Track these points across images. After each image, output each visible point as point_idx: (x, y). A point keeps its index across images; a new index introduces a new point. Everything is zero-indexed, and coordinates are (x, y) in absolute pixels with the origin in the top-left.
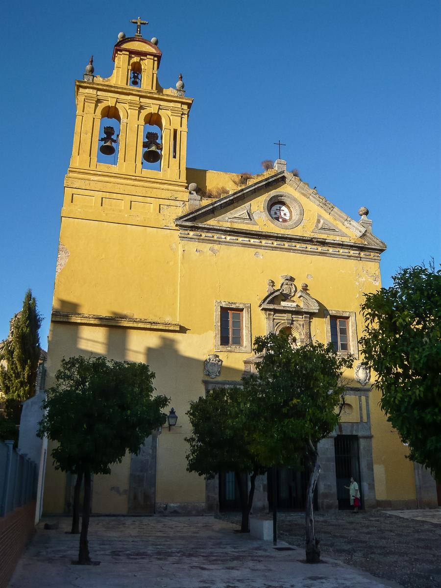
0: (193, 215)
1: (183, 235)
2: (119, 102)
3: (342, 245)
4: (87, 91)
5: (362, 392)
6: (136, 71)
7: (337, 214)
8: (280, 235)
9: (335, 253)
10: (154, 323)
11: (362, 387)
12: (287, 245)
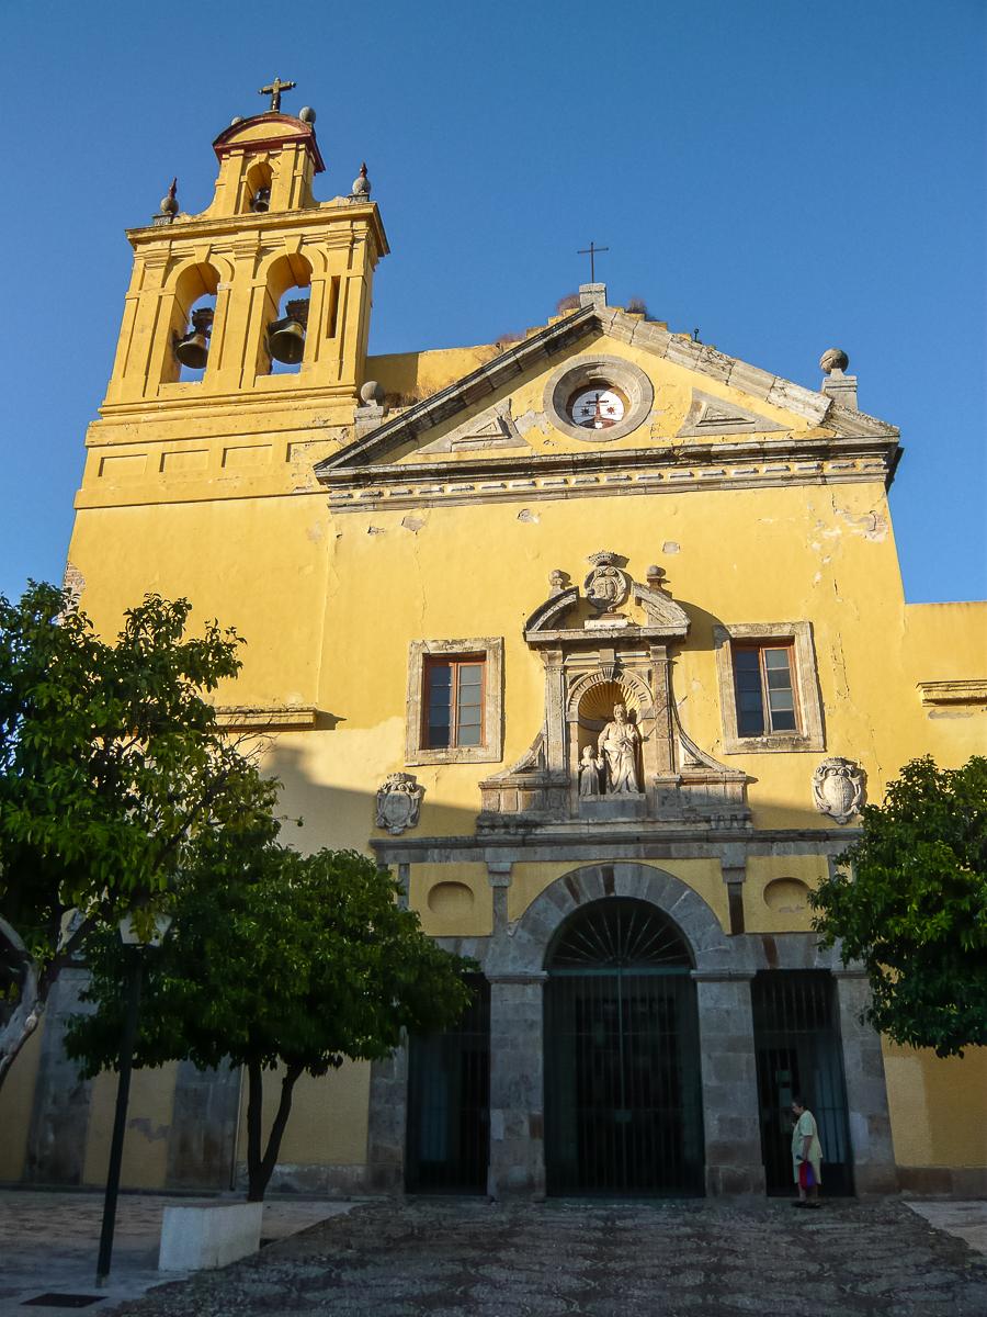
0: (359, 450)
1: (338, 502)
2: (216, 253)
3: (761, 453)
4: (152, 246)
6: (258, 191)
7: (746, 378)
8: (581, 457)
9: (745, 475)
10: (251, 711)
11: (838, 827)
12: (604, 479)
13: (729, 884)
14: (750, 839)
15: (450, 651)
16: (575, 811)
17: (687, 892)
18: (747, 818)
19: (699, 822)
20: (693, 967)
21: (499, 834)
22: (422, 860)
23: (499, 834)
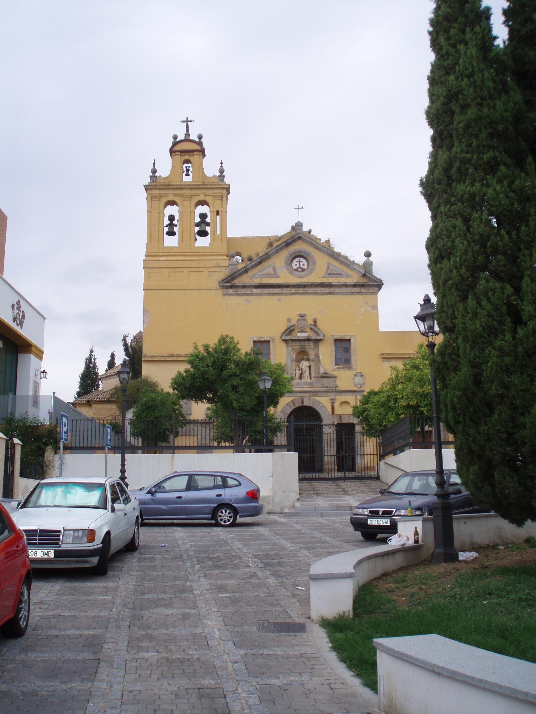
5: (358, 393)
18: (336, 387)
20: (322, 422)
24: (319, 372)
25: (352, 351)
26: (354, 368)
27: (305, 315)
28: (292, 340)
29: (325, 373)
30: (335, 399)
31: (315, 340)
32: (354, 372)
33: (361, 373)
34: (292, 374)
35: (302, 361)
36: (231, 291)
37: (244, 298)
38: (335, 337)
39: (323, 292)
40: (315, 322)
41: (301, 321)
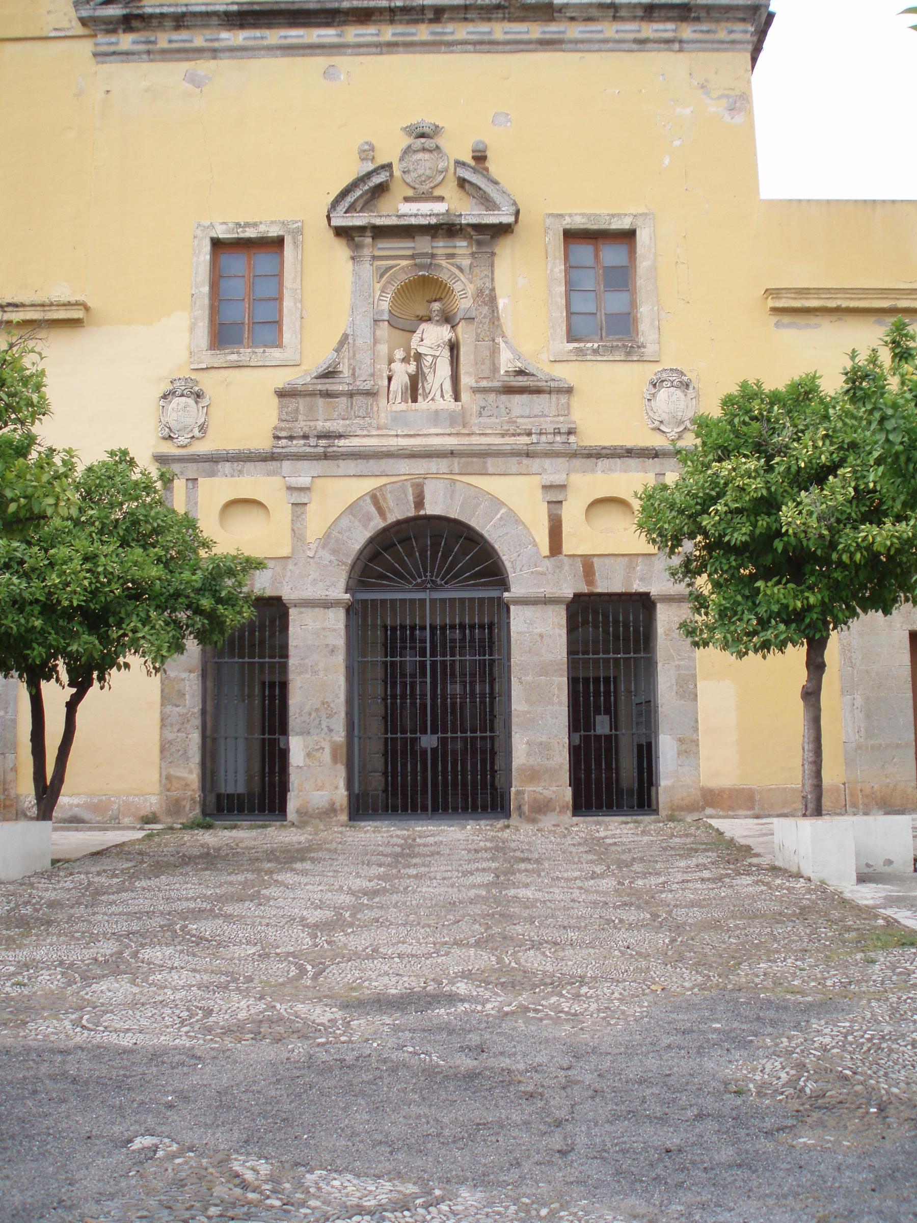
13: (548, 502)
14: (574, 455)
15: (242, 235)
16: (383, 421)
17: (503, 511)
18: (570, 433)
19: (519, 435)
20: (507, 589)
21: (298, 446)
22: (212, 474)
23: (298, 446)
24: (495, 369)
25: (640, 282)
26: (650, 350)
27: (437, 130)
28: (380, 232)
29: (521, 372)
30: (563, 487)
31: (479, 228)
32: (650, 371)
33: (682, 374)
34: (373, 375)
35: (424, 326)
36: (126, 41)
37: (182, 67)
38: (567, 223)
39: (518, 37)
40: (480, 158)
41: (420, 156)
